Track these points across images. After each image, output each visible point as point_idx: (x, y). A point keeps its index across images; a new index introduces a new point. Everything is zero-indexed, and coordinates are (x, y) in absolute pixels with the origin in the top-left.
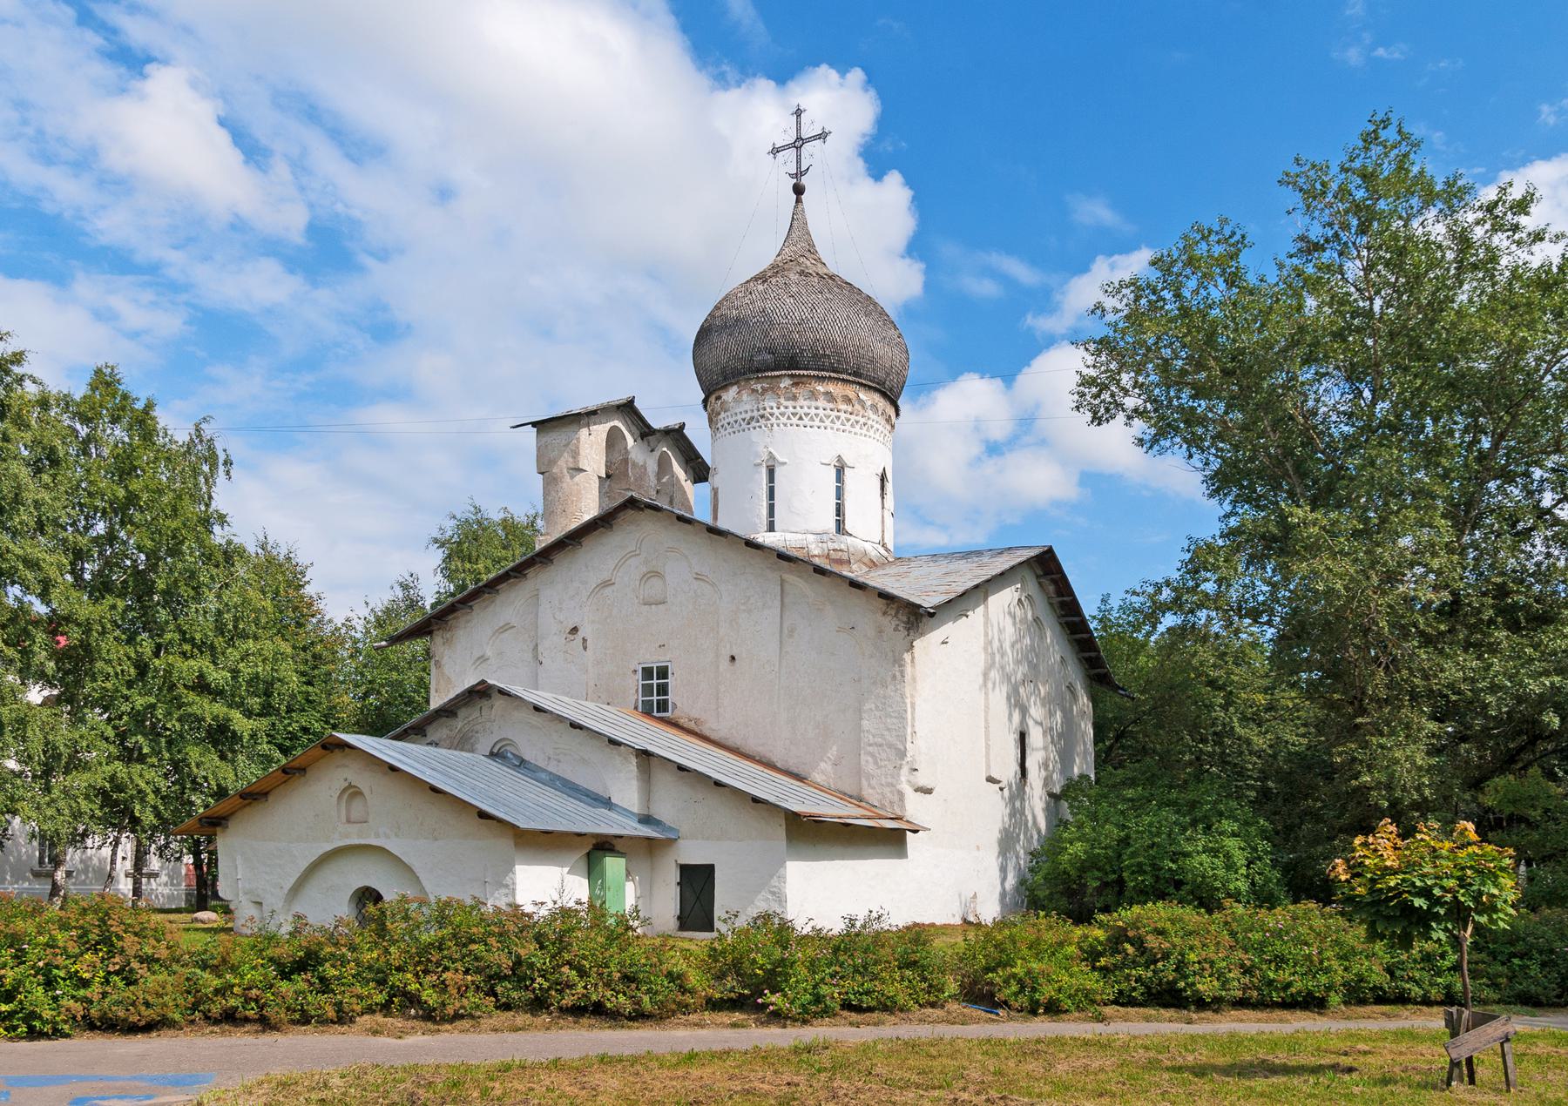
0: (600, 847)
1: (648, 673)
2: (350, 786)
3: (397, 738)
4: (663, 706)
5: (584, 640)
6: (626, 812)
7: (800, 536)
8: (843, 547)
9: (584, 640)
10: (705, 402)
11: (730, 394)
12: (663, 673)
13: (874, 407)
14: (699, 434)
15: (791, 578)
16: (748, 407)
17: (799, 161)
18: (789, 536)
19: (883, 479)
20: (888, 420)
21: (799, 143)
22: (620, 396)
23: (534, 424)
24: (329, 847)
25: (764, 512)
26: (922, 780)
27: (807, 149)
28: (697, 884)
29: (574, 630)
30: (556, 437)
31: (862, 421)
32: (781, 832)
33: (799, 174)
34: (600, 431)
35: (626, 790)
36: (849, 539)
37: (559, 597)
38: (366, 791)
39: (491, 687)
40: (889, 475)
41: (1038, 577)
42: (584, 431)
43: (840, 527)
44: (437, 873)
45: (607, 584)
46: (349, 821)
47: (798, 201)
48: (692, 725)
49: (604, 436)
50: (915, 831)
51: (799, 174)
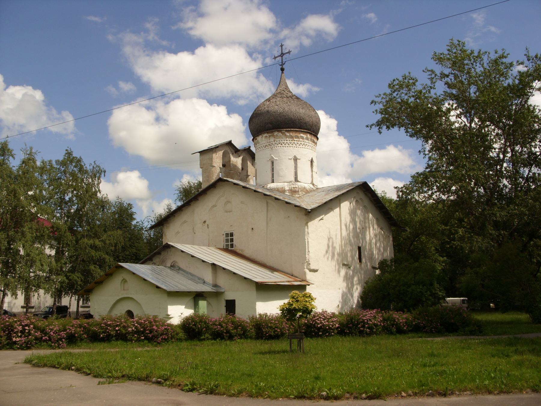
0: (198, 296)
1: (227, 235)
2: (124, 279)
3: (142, 263)
4: (232, 246)
5: (208, 225)
6: (208, 284)
7: (282, 184)
8: (297, 186)
9: (208, 225)
10: (253, 140)
11: (259, 138)
12: (232, 235)
13: (307, 139)
14: (253, 149)
15: (270, 201)
16: (265, 142)
17: (282, 60)
18: (278, 184)
19: (312, 161)
20: (314, 142)
21: (282, 55)
22: (227, 140)
23: (199, 152)
24: (118, 298)
25: (271, 176)
26: (312, 267)
27: (284, 57)
28: (231, 306)
29: (205, 222)
30: (206, 157)
31: (303, 143)
32: (254, 288)
33: (282, 64)
34: (220, 153)
35: (208, 276)
36: (299, 183)
37: (202, 211)
38: (128, 280)
39: (169, 245)
40: (314, 160)
41: (364, 192)
42: (214, 155)
43: (296, 180)
44: (146, 307)
45: (214, 206)
46: (124, 290)
47: (282, 73)
48: (240, 252)
49: (222, 154)
50: (309, 285)
51: (282, 64)
